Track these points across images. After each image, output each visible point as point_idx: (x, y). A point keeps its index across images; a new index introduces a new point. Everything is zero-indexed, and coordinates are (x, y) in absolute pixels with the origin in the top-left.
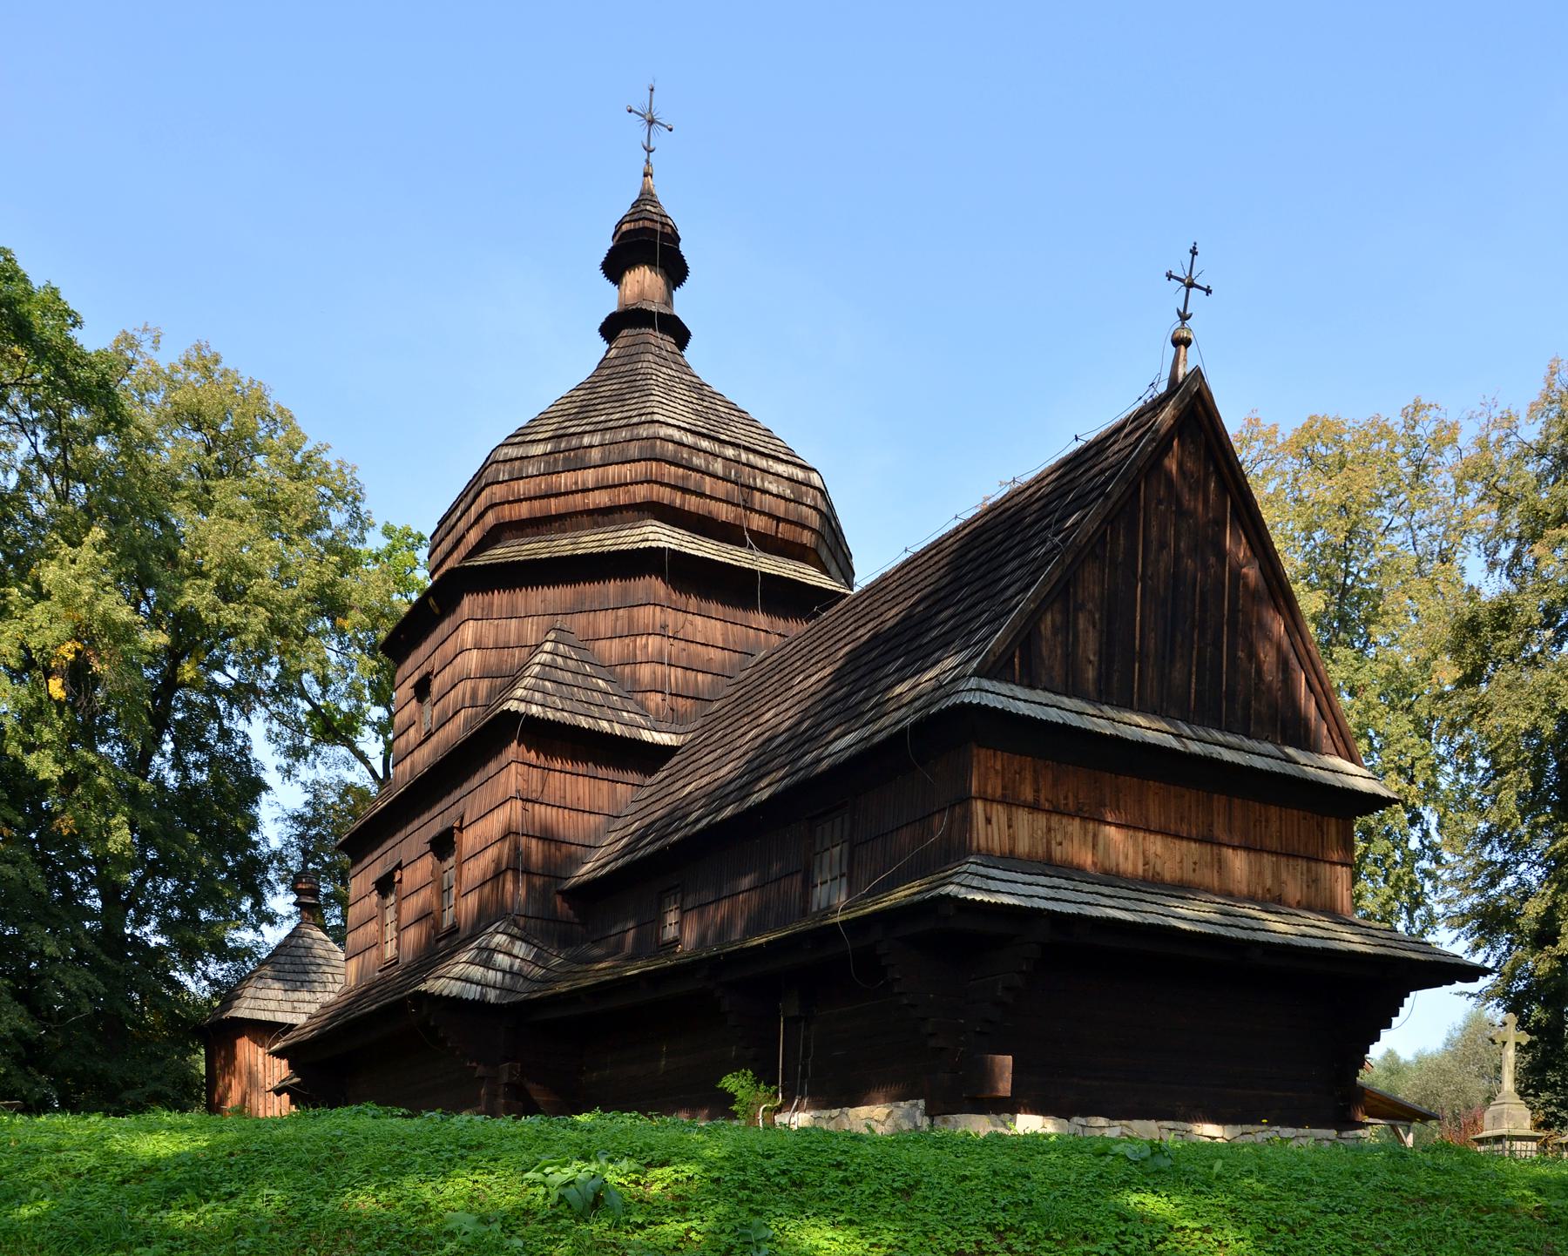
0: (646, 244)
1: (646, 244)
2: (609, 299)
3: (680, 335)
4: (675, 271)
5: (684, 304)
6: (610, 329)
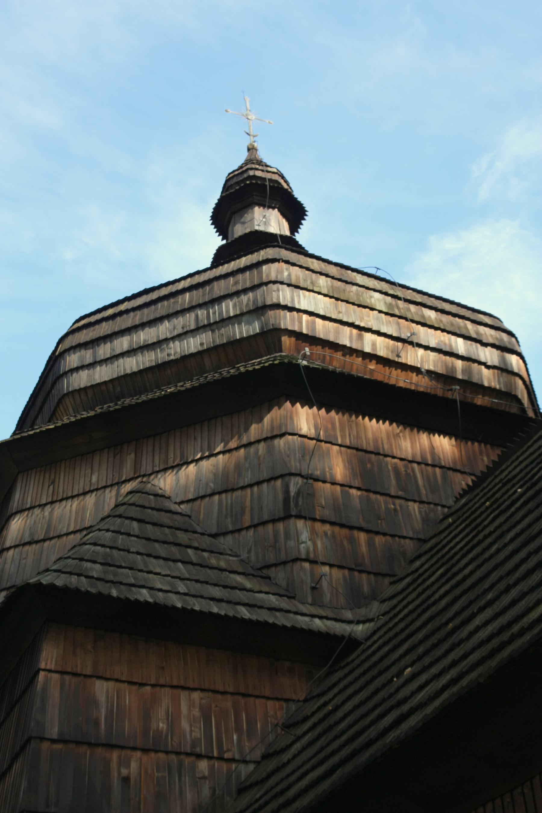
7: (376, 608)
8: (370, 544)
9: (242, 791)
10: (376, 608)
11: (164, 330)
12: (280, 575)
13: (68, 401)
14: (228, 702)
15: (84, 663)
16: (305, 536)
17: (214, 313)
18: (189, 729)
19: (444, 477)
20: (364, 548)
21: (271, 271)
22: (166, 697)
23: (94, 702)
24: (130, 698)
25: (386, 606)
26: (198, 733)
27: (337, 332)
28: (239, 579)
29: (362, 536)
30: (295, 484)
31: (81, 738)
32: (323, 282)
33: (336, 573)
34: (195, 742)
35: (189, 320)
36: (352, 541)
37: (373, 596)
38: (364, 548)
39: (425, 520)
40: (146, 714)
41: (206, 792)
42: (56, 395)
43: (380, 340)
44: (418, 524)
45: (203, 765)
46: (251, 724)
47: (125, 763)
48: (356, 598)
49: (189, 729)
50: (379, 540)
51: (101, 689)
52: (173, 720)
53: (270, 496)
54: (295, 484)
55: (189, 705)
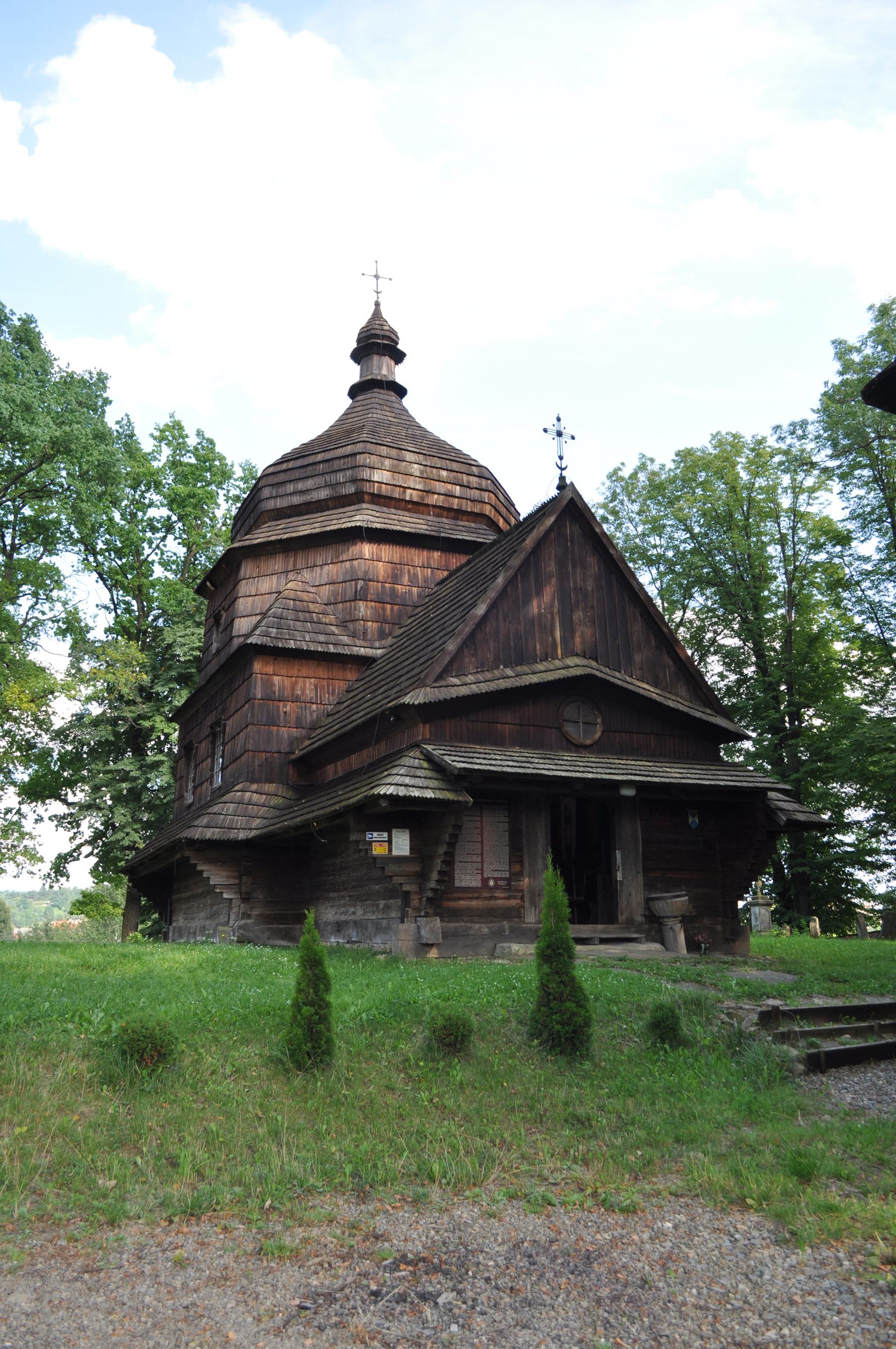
0: (377, 344)
1: (377, 344)
2: (353, 374)
3: (401, 392)
4: (398, 357)
5: (401, 374)
6: (354, 392)
7: (390, 641)
8: (392, 610)
9: (328, 716)
10: (390, 641)
11: (310, 483)
12: (351, 626)
13: (265, 514)
14: (325, 683)
15: (270, 669)
16: (363, 609)
17: (333, 479)
18: (310, 693)
19: (432, 573)
20: (388, 612)
21: (360, 459)
22: (301, 680)
23: (273, 685)
24: (287, 682)
25: (395, 640)
26: (313, 695)
27: (392, 491)
28: (333, 628)
29: (389, 606)
30: (360, 583)
31: (269, 697)
32: (387, 462)
33: (375, 625)
34: (311, 698)
35: (320, 481)
36: (384, 609)
37: (390, 634)
38: (388, 612)
39: (419, 596)
40: (293, 689)
41: (315, 716)
42: (256, 500)
43: (414, 492)
44: (415, 598)
45: (314, 706)
46: (333, 690)
47: (285, 706)
48: (382, 635)
49: (310, 693)
50: (396, 607)
51: (276, 679)
52: (303, 690)
53: (350, 588)
54: (360, 583)
55: (310, 684)
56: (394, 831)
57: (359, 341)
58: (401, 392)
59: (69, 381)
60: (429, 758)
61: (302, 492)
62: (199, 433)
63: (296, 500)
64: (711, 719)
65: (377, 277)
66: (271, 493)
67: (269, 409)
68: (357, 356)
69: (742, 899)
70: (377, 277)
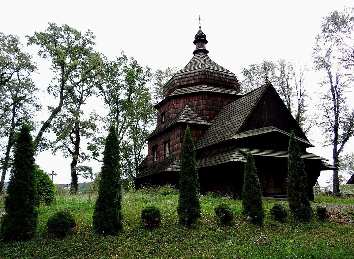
0: (200, 39)
1: (200, 39)
2: (194, 48)
3: (207, 52)
6: (195, 53)
8: (213, 112)
36: (211, 112)
56: (102, 163)
57: (196, 38)
58: (207, 52)
59: (177, 90)
60: (240, 152)
61: (186, 81)
62: (132, 58)
63: (185, 83)
64: (305, 142)
65: (200, 20)
66: (178, 81)
67: (176, 58)
68: (195, 43)
69: (315, 185)
70: (200, 20)
